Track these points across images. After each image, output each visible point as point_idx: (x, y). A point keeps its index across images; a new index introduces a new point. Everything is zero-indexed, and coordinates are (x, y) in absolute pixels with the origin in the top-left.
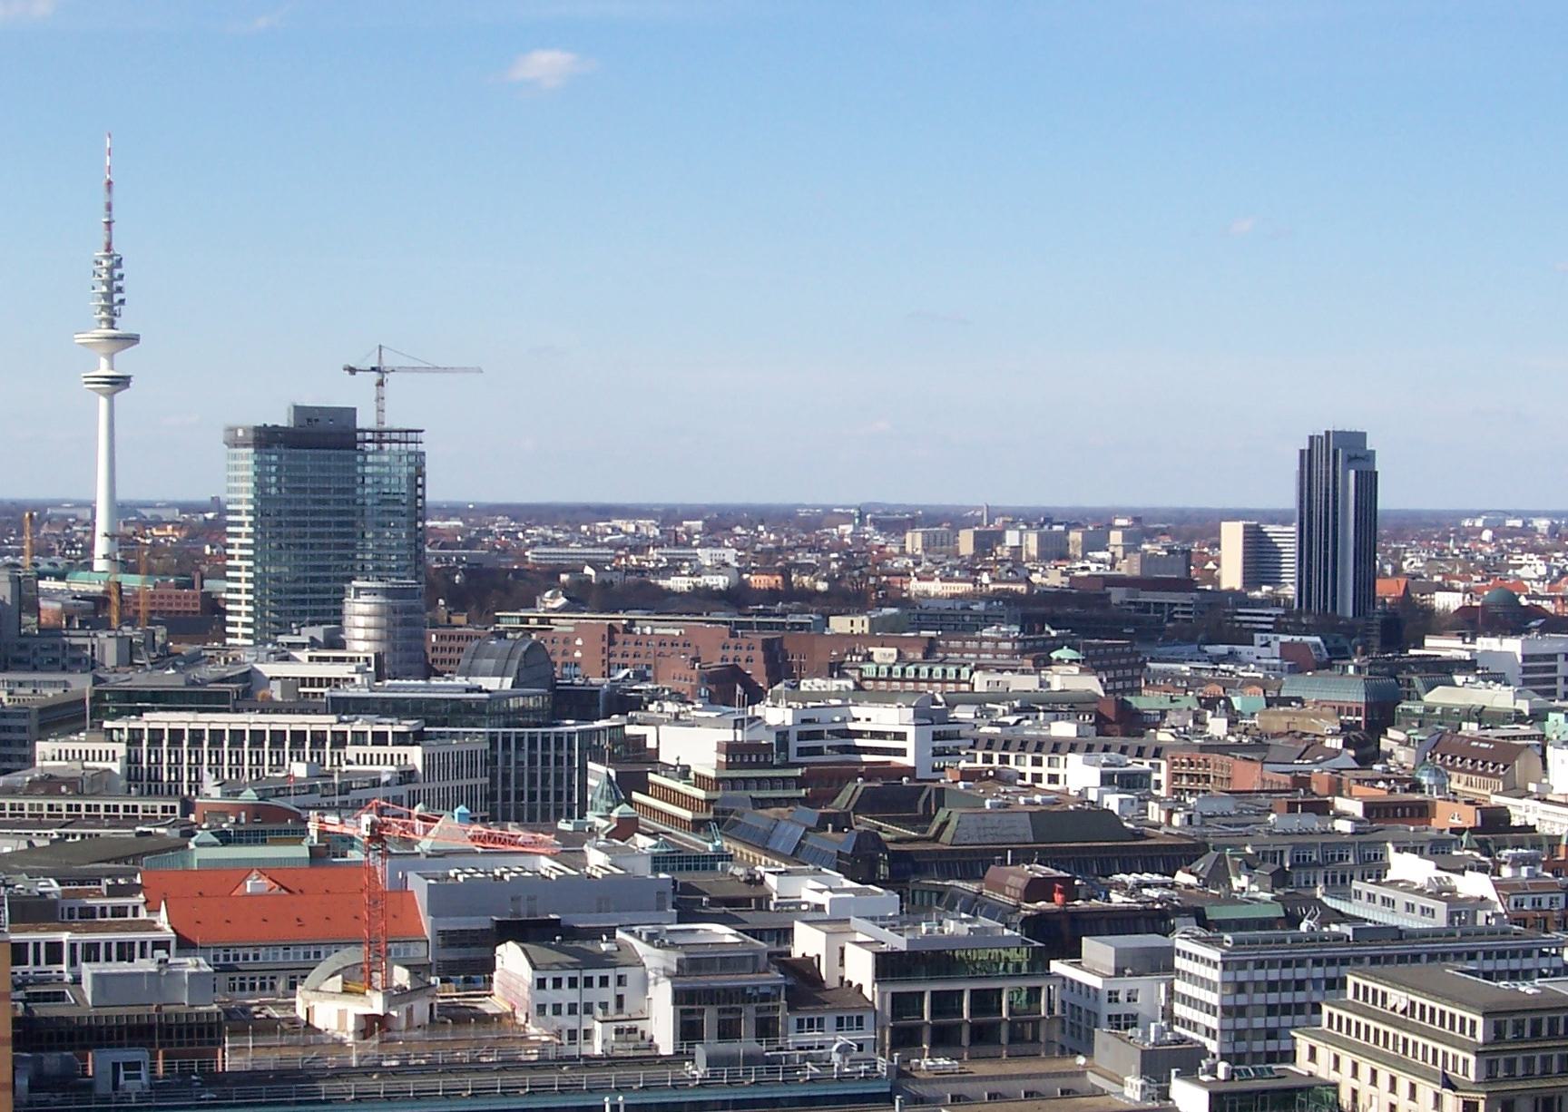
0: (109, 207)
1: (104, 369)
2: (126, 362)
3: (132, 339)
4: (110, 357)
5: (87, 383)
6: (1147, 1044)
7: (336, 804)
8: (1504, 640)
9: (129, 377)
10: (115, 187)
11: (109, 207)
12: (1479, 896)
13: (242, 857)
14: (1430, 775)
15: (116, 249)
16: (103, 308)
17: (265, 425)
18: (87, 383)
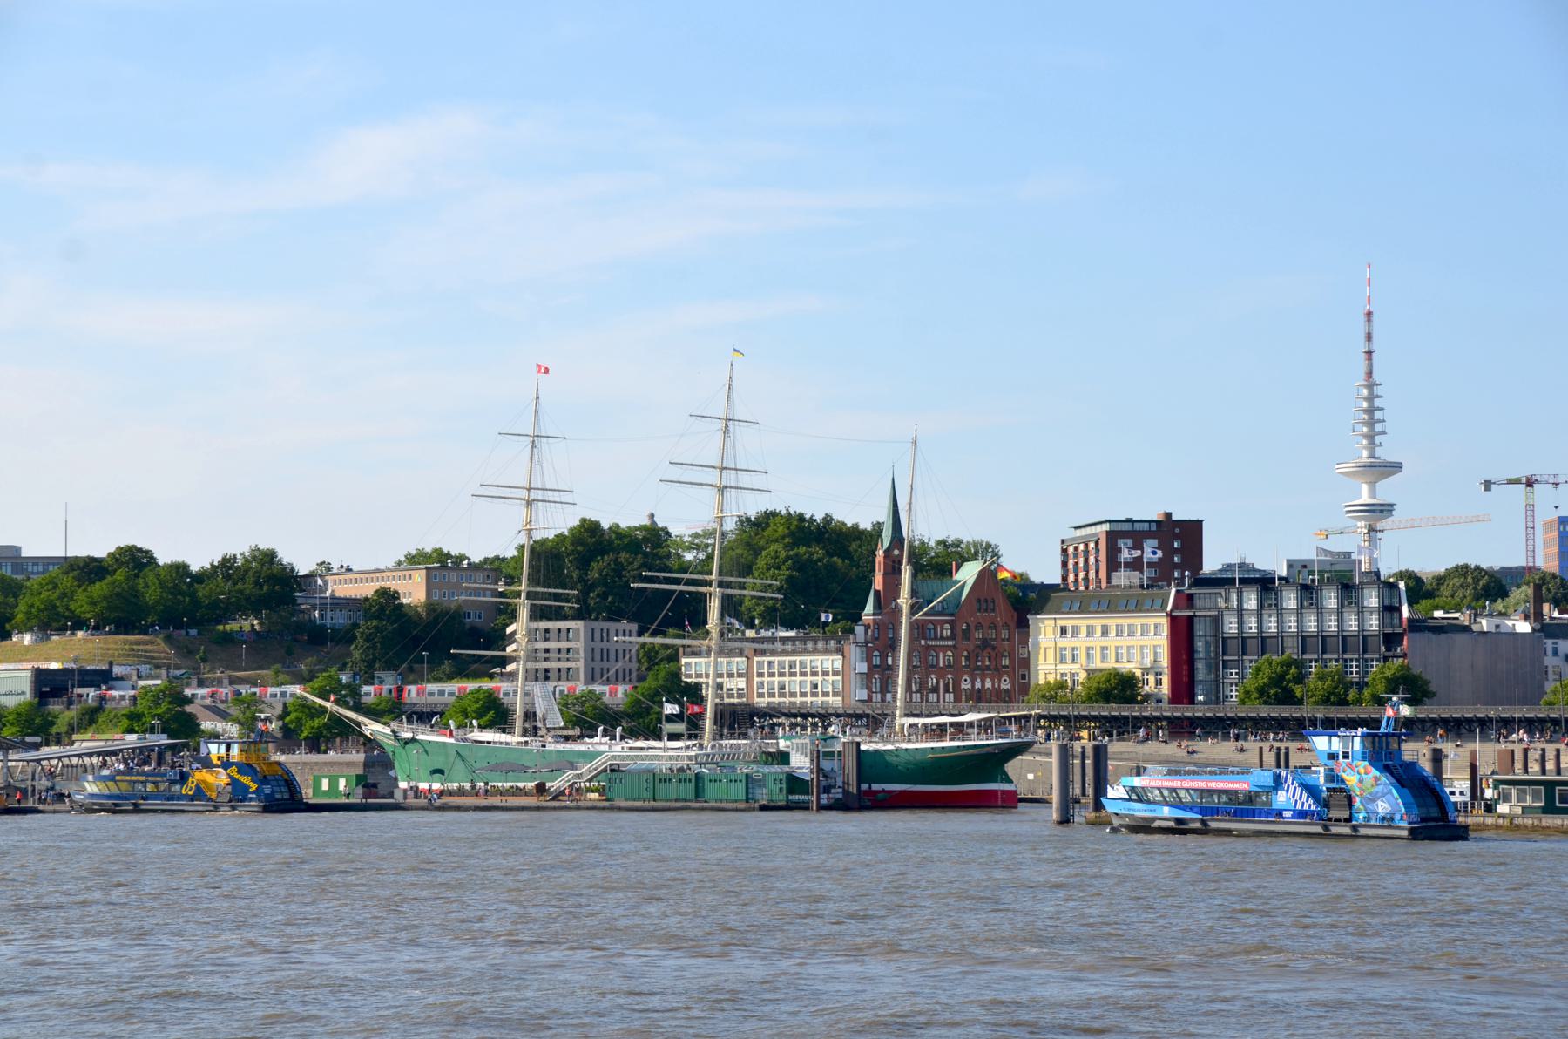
0: (1369, 337)
1: (1365, 499)
2: (1387, 490)
3: (1396, 467)
4: (1372, 484)
5: (1349, 512)
6: (686, 611)
7: (1013, 728)
8: (646, 522)
9: (1392, 505)
10: (1375, 317)
11: (1369, 337)
12: (446, 551)
13: (360, 813)
14: (937, 555)
15: (1376, 377)
16: (1365, 423)
17: (765, 512)
18: (1349, 512)
